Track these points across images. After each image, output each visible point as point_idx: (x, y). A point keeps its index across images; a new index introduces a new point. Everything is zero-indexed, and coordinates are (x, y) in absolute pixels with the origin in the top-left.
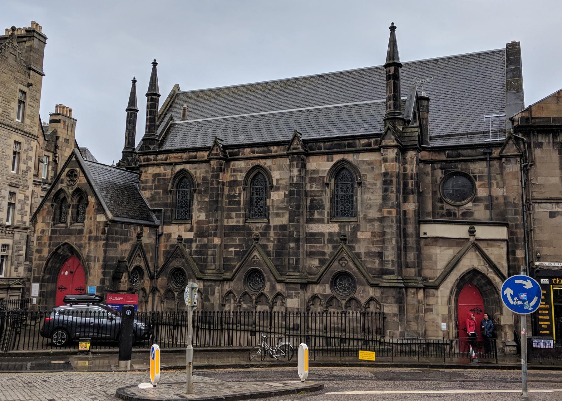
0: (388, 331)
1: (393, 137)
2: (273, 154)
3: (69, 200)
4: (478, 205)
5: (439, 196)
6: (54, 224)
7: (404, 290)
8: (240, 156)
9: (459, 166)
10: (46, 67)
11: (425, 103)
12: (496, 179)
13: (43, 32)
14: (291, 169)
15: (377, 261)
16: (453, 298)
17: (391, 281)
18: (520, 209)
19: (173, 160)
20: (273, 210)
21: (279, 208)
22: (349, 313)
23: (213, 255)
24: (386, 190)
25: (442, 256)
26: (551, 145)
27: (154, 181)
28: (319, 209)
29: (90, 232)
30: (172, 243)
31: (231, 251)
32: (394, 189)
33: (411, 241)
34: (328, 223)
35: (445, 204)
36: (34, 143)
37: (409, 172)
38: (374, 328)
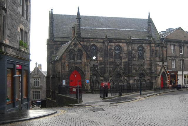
21: (124, 57)
29: (85, 63)
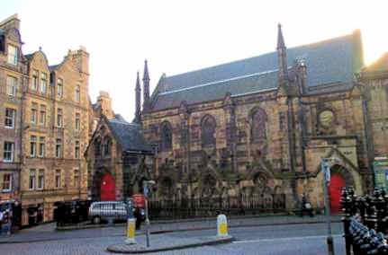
3: (102, 142)
13: (87, 51)
15: (279, 164)
18: (363, 127)
24: (281, 122)
36: (87, 114)
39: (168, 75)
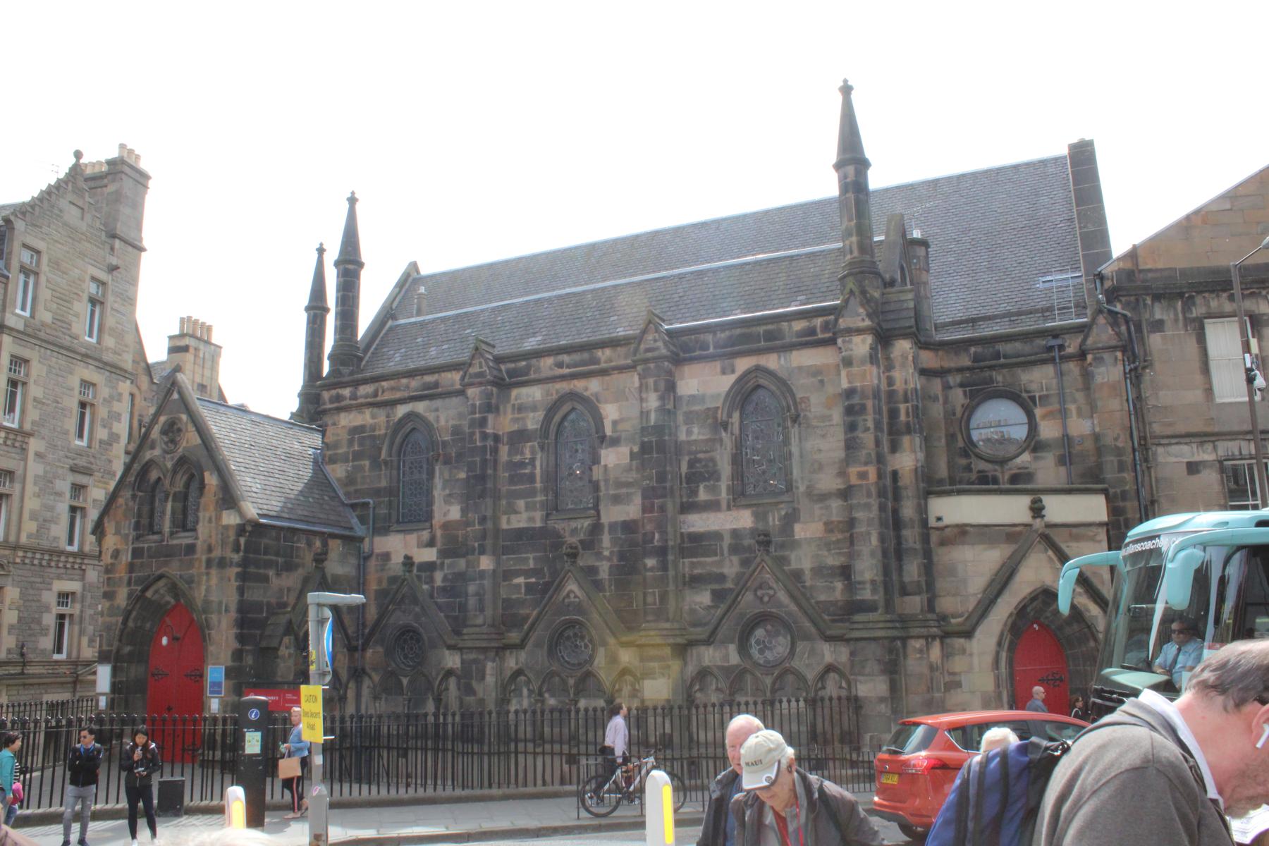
0: (867, 737)
1: (861, 310)
2: (603, 365)
4: (1042, 458)
5: (961, 444)
6: (138, 538)
7: (899, 643)
8: (532, 376)
9: (1000, 378)
10: (150, 234)
11: (921, 251)
12: (1075, 401)
13: (144, 165)
14: (644, 395)
15: (839, 585)
16: (1004, 655)
17: (871, 625)
18: (1128, 459)
19: (387, 396)
20: (607, 489)
21: (619, 484)
22: (781, 702)
23: (477, 594)
24: (851, 427)
25: (975, 566)
26: (1181, 324)
27: (351, 442)
28: (708, 480)
29: (210, 549)
30: (392, 573)
31: (518, 586)
32: (870, 424)
33: (911, 536)
34: (729, 508)
35: (973, 459)
36: (125, 387)
37: (899, 386)
38: (837, 731)
39: (425, 270)
